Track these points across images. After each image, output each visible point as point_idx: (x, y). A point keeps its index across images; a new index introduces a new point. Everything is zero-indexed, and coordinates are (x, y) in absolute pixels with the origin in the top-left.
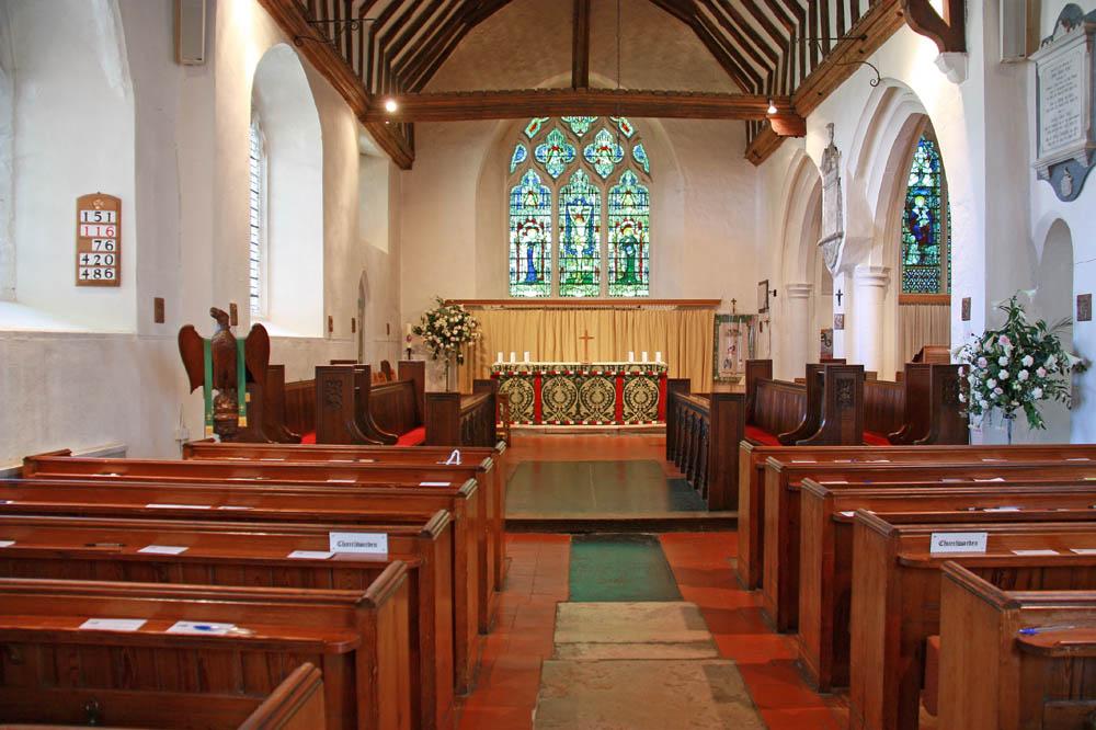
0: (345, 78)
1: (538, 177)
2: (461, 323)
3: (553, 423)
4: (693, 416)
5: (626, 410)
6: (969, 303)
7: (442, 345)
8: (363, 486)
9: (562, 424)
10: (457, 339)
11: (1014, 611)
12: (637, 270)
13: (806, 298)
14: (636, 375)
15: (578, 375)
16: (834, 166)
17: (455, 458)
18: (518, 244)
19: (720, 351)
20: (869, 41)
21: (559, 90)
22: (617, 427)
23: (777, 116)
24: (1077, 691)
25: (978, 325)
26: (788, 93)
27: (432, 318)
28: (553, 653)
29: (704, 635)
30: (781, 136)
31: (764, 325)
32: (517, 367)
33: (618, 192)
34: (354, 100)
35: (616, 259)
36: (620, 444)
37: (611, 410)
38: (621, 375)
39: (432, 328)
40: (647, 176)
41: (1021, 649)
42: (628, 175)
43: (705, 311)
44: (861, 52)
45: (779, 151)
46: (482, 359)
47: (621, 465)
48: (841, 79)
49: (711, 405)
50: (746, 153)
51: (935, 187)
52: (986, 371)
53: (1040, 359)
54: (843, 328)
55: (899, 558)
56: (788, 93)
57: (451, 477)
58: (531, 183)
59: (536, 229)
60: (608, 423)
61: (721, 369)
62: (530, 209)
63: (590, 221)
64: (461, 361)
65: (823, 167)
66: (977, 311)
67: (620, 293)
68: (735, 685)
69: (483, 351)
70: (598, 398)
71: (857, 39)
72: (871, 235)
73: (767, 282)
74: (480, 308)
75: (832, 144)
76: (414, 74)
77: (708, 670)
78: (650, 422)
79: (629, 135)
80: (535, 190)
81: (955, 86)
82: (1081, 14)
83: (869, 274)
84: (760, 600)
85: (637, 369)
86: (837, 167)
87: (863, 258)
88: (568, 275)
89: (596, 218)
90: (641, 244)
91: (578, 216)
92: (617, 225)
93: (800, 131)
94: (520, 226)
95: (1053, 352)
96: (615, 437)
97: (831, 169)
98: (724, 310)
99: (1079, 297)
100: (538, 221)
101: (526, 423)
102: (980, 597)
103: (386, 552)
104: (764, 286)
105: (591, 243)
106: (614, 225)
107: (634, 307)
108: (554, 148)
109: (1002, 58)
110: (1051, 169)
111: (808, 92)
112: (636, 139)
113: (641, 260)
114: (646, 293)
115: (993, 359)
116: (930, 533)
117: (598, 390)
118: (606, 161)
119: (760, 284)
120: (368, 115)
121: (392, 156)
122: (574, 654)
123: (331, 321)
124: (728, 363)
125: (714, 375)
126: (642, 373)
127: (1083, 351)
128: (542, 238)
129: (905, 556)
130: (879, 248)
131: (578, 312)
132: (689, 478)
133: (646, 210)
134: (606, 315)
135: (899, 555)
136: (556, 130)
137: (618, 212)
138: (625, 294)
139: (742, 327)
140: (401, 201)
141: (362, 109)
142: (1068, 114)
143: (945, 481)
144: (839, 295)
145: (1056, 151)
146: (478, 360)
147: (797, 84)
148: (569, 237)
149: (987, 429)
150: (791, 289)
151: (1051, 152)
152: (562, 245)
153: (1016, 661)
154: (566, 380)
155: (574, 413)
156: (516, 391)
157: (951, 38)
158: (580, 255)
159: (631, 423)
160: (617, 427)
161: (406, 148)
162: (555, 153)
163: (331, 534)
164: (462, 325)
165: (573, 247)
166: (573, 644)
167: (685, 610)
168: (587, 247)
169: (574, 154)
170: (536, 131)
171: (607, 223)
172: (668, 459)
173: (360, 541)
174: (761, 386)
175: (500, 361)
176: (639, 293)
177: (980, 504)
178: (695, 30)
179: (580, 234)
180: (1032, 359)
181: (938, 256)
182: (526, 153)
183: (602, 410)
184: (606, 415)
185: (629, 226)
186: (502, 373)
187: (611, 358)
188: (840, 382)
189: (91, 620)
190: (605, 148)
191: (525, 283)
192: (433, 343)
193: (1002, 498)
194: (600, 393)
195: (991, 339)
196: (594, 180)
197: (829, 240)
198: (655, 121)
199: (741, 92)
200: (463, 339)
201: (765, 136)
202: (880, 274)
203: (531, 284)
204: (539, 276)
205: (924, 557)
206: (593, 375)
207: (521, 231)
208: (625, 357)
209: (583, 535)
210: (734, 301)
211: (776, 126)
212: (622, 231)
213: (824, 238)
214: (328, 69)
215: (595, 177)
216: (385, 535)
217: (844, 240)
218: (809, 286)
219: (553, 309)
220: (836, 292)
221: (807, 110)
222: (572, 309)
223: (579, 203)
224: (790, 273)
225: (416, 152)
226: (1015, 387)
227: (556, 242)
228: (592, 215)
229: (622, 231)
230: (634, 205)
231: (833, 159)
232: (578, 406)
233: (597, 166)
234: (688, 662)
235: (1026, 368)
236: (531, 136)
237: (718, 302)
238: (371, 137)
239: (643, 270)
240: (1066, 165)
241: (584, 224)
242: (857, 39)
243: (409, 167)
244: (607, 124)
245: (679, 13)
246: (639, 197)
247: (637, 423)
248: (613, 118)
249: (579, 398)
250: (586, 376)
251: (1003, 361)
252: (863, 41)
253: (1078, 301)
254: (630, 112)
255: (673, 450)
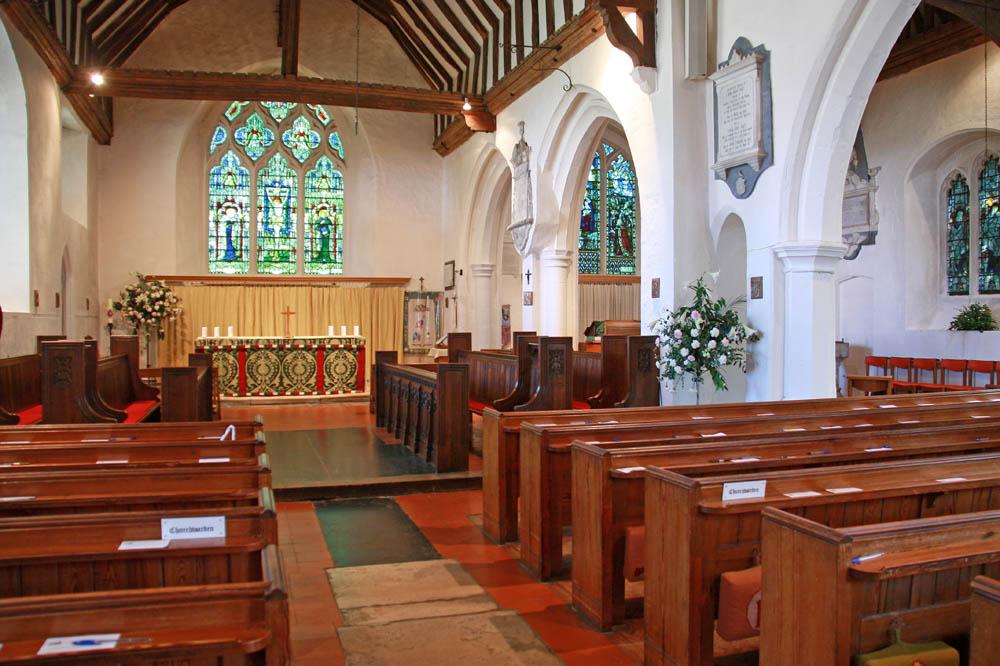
0: (51, 45)
1: (237, 159)
2: (163, 298)
3: (257, 394)
4: (400, 382)
5: (327, 381)
6: (659, 283)
7: (143, 320)
8: (139, 466)
9: (266, 395)
10: (159, 314)
11: (848, 544)
12: (331, 249)
13: (489, 277)
14: (335, 348)
15: (281, 348)
16: (524, 160)
17: (230, 433)
18: (217, 222)
19: (410, 323)
20: (564, 51)
21: (269, 75)
22: (319, 397)
23: (471, 113)
24: (882, 607)
25: (668, 301)
26: (479, 92)
27: (133, 294)
28: (341, 617)
29: (477, 590)
30: (474, 131)
31: (451, 302)
32: (221, 341)
33: (314, 175)
34: (57, 68)
35: (312, 239)
36: (322, 413)
37: (313, 381)
38: (321, 348)
39: (132, 304)
40: (342, 163)
41: (853, 575)
42: (324, 160)
43: (396, 288)
44: (555, 60)
45: (467, 144)
46: (183, 334)
47: (322, 434)
48: (534, 82)
49: (438, 376)
50: (434, 144)
51: (596, 182)
52: (680, 341)
53: (724, 330)
54: (531, 304)
55: (700, 507)
56: (479, 92)
57: (227, 452)
58: (230, 164)
59: (235, 208)
60: (310, 394)
61: (410, 343)
62: (229, 189)
63: (287, 203)
64: (161, 336)
65: (514, 160)
66: (667, 290)
67: (315, 271)
68: (526, 633)
69: (183, 325)
70: (300, 369)
71: (552, 48)
72: (557, 221)
73: (453, 262)
74: (181, 284)
75: (522, 140)
76: (115, 49)
77: (494, 620)
78: (349, 392)
79: (325, 122)
80: (234, 171)
81: (646, 96)
82: (751, 46)
83: (556, 256)
84: (516, 551)
85: (337, 342)
86: (528, 161)
87: (550, 242)
88: (265, 254)
89: (293, 200)
90: (336, 225)
91: (276, 198)
92: (313, 207)
93: (490, 126)
94: (219, 206)
95: (734, 325)
96: (316, 406)
97: (521, 163)
98: (413, 287)
99: (752, 279)
100: (237, 201)
101: (231, 395)
102: (814, 535)
103: (223, 535)
104: (451, 266)
105: (288, 223)
106: (310, 207)
107: (330, 284)
108: (254, 132)
109: (687, 76)
110: (728, 171)
111: (501, 92)
112: (332, 127)
113: (335, 240)
114: (340, 271)
115: (686, 331)
116: (722, 484)
117: (300, 362)
118: (302, 146)
119: (446, 264)
120: (71, 87)
121: (90, 129)
122: (364, 619)
123: (36, 296)
124: (417, 336)
125: (404, 347)
126: (342, 346)
127: (755, 324)
128: (241, 217)
129: (705, 504)
130: (564, 234)
131: (277, 288)
132: (407, 442)
133: (340, 194)
134: (303, 291)
135: (700, 504)
136: (256, 114)
137: (314, 195)
138: (320, 272)
139: (429, 302)
140: (100, 177)
141: (66, 79)
142: (743, 127)
143: (678, 437)
144: (528, 275)
145: (734, 156)
146: (178, 334)
147: (490, 85)
148: (267, 218)
149: (676, 392)
150: (477, 269)
151: (726, 158)
152: (260, 225)
153: (848, 587)
154: (270, 354)
155: (278, 385)
156: (221, 365)
157: (644, 54)
158: (277, 234)
159: (332, 393)
160: (319, 397)
161: (106, 122)
162: (255, 136)
163: (163, 521)
164: (164, 301)
165: (270, 226)
166: (359, 608)
167: (448, 567)
168: (284, 227)
169: (273, 138)
170: (235, 115)
171: (303, 203)
172: (378, 426)
173: (197, 526)
174: (461, 356)
175: (204, 335)
176: (334, 271)
177: (727, 456)
178: (391, 31)
179: (278, 214)
180: (718, 331)
181: (598, 241)
182: (225, 136)
183: (268, 382)
184: (307, 386)
185: (324, 208)
186: (207, 347)
187: (309, 330)
188: (552, 352)
189: (49, 641)
190: (302, 135)
191: (225, 260)
192: (134, 318)
193: (745, 450)
194: (303, 364)
195: (685, 314)
196: (292, 164)
197: (519, 226)
198: (351, 111)
199: (429, 88)
200: (165, 314)
201: (456, 129)
202: (564, 256)
203: (230, 261)
204: (238, 254)
205: (714, 505)
206: (295, 348)
207: (220, 211)
208: (323, 331)
209: (323, 502)
210: (422, 279)
211: (470, 121)
212: (318, 212)
213: (513, 223)
214: (31, 32)
215: (293, 162)
216: (223, 518)
217: (534, 225)
218: (492, 266)
219: (253, 286)
220: (525, 272)
221: (498, 108)
222: (271, 286)
223: (277, 184)
224: (474, 253)
225: (115, 127)
226: (704, 355)
227: (254, 222)
228: (289, 197)
229: (318, 212)
230: (329, 189)
231: (524, 153)
232: (281, 378)
233: (294, 151)
234: (474, 616)
235: (714, 338)
236: (231, 118)
237: (407, 280)
238: (72, 109)
239: (243, 248)
240: (741, 168)
241: (281, 205)
242: (552, 48)
243: (107, 143)
244: (304, 112)
245: (377, 13)
246: (333, 181)
247: (337, 393)
248: (262, 103)
249: (282, 370)
250: (288, 349)
251: (694, 333)
252: (558, 50)
253: (752, 282)
254: (324, 100)
255: (383, 417)
